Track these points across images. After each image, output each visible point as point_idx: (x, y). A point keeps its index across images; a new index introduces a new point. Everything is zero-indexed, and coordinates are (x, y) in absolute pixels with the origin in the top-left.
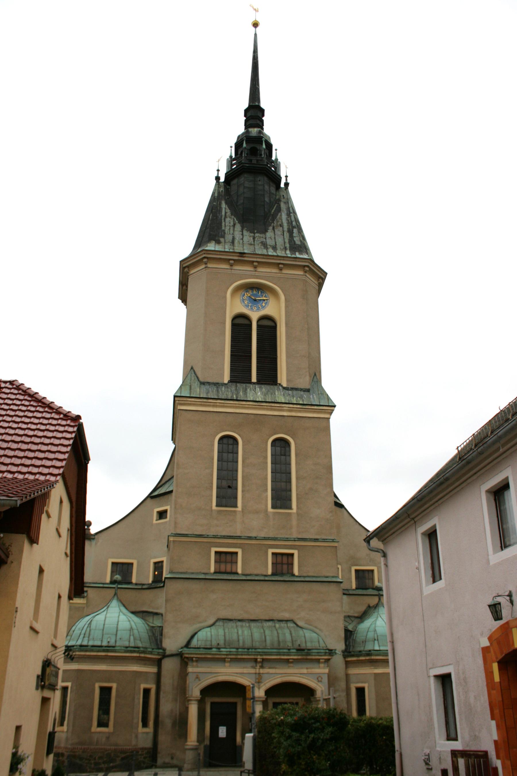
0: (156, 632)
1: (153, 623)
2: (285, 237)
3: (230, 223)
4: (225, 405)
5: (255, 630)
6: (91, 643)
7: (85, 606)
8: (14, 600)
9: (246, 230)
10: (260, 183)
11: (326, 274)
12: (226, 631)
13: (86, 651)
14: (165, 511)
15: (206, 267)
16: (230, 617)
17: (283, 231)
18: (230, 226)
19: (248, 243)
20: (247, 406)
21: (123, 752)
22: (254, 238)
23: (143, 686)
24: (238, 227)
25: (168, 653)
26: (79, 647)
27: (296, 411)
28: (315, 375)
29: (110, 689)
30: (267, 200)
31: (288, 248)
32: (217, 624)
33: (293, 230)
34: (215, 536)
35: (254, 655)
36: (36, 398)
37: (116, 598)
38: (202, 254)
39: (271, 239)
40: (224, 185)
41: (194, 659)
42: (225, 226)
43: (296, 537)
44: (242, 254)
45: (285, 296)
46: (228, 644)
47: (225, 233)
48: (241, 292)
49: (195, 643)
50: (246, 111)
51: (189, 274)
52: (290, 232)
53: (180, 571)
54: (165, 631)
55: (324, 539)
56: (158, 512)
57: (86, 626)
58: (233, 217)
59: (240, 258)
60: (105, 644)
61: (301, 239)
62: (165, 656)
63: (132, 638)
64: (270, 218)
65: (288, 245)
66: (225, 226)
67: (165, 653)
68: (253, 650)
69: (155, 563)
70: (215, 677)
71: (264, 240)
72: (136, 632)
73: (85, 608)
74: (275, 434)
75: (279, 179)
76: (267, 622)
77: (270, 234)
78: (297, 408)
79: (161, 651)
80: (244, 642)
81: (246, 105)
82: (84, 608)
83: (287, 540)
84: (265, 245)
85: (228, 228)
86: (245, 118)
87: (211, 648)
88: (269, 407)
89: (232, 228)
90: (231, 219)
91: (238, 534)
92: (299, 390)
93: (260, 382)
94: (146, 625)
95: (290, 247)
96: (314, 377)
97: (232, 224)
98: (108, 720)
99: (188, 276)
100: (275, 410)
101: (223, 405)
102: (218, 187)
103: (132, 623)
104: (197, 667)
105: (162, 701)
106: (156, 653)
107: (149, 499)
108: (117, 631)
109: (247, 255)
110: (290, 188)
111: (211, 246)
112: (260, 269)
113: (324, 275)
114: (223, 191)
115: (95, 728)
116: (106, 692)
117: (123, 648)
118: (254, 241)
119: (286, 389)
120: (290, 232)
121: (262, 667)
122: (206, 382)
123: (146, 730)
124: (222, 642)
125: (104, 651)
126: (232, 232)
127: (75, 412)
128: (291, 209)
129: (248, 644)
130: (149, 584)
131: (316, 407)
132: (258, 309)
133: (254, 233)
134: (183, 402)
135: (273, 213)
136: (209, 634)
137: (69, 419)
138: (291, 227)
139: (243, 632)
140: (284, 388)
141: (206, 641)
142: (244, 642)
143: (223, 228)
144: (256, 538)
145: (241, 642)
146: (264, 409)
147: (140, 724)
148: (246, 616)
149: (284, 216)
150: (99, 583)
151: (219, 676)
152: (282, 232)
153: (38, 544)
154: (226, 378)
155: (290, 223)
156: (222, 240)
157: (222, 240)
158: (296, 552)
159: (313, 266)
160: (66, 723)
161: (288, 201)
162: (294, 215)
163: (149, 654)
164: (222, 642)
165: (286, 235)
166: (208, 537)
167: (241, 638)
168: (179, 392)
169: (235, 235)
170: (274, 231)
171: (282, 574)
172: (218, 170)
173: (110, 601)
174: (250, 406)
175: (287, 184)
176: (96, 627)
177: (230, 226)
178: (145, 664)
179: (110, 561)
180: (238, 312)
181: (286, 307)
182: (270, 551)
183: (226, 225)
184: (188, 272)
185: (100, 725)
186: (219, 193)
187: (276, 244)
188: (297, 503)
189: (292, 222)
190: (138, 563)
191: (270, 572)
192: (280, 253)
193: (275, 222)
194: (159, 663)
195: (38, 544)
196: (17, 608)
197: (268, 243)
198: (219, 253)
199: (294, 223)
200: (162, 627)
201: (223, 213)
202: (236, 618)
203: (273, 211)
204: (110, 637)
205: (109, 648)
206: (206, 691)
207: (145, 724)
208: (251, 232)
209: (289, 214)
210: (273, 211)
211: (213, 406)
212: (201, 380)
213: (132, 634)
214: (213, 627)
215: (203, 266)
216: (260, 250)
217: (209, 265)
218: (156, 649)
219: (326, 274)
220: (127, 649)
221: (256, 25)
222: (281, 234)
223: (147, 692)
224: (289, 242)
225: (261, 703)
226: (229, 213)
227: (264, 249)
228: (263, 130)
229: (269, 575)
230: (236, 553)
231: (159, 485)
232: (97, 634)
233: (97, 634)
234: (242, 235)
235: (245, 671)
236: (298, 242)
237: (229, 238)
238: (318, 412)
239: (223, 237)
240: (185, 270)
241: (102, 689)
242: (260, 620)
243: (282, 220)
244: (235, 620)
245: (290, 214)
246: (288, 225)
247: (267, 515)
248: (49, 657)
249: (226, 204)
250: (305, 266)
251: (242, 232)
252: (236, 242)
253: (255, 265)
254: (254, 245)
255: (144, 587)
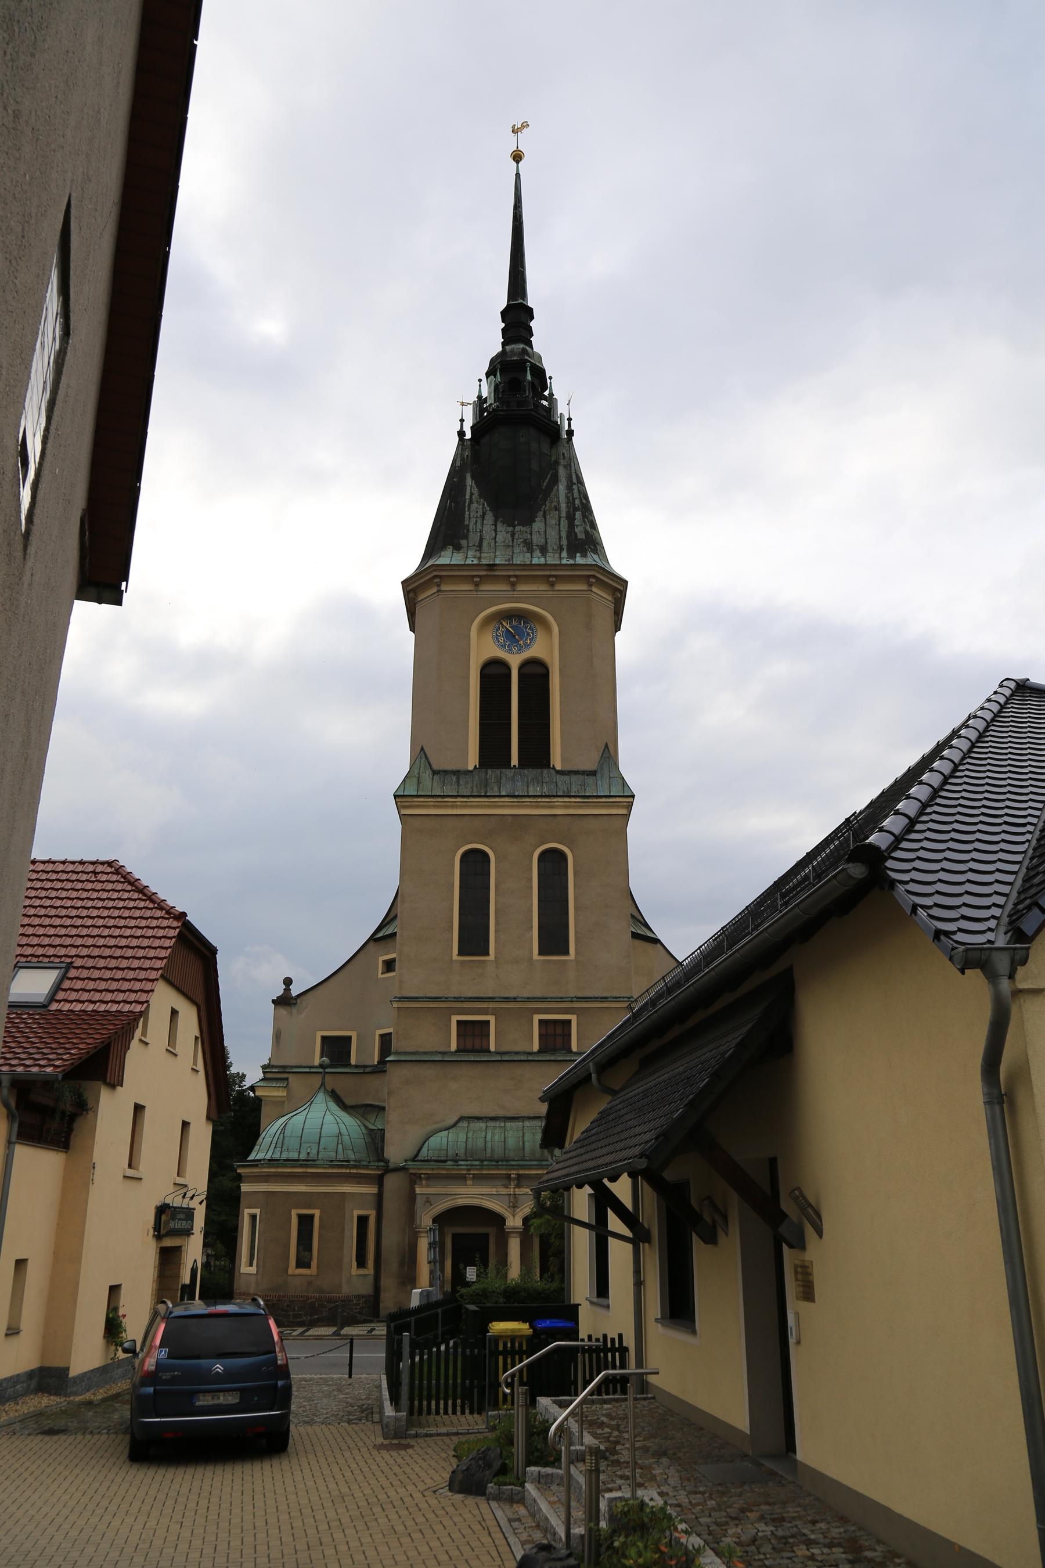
0: (375, 1137)
1: (374, 1124)
2: (562, 529)
3: (477, 512)
4: (469, 804)
5: (510, 1134)
6: (284, 1156)
7: (285, 1099)
8: (91, 1155)
9: (501, 522)
10: (522, 440)
11: (627, 582)
12: (470, 1135)
13: (278, 1167)
14: (393, 960)
15: (438, 591)
16: (477, 1114)
17: (560, 518)
18: (477, 517)
19: (503, 544)
20: (500, 804)
21: (330, 1300)
22: (513, 535)
23: (356, 1213)
24: (489, 518)
25: (391, 1165)
26: (267, 1162)
27: (573, 807)
28: (606, 746)
29: (311, 1217)
30: (535, 466)
31: (565, 547)
32: (460, 1124)
33: (575, 515)
34: (457, 998)
35: (506, 1169)
36: (136, 888)
37: (322, 1089)
38: (431, 572)
39: (539, 533)
40: (471, 445)
41: (422, 1176)
42: (470, 518)
43: (574, 996)
44: (491, 567)
45: (558, 625)
46: (470, 1154)
47: (468, 531)
48: (494, 625)
49: (424, 1153)
50: (504, 314)
51: (416, 602)
52: (571, 518)
53: (408, 1050)
54: (387, 1135)
55: (616, 998)
56: (384, 961)
57: (279, 1131)
58: (482, 500)
59: (489, 573)
60: (303, 1156)
61: (588, 528)
62: (388, 1170)
63: (340, 1146)
64: (540, 497)
65: (564, 542)
66: (470, 518)
67: (388, 1166)
68: (504, 1163)
69: (382, 1036)
70: (453, 1199)
71: (529, 536)
72: (346, 1138)
73: (286, 1102)
74: (543, 843)
75: (557, 428)
76: (531, 1120)
77: (538, 525)
78: (575, 802)
79: (382, 1164)
80: (492, 1150)
81: (503, 304)
82: (284, 1102)
83: (561, 1000)
84: (529, 546)
85: (473, 520)
86: (503, 325)
87: (445, 1161)
88: (533, 804)
89: (479, 521)
90: (480, 504)
91: (490, 995)
92: (580, 774)
93: (523, 763)
94: (362, 1128)
95: (567, 545)
96: (604, 750)
97: (480, 513)
98: (311, 1259)
99: (415, 604)
100: (543, 807)
101: (465, 804)
102: (462, 450)
103: (342, 1126)
104: (428, 1186)
105: (385, 1233)
106: (375, 1167)
107: (371, 944)
108: (320, 1137)
109: (498, 568)
110: (575, 439)
111: (446, 558)
112: (521, 587)
113: (622, 585)
114: (470, 455)
115: (292, 1269)
116: (306, 1221)
117: (326, 1162)
118: (513, 541)
119: (560, 774)
120: (571, 518)
121: (518, 1186)
122: (441, 771)
123: (362, 1271)
124: (462, 1152)
125: (301, 1166)
126: (479, 527)
127: (180, 909)
128: (574, 476)
129: (499, 1153)
130: (373, 1066)
131: (604, 800)
132: (520, 649)
133: (514, 526)
134: (407, 804)
135: (546, 487)
136: (445, 1140)
137: (171, 918)
138: (572, 510)
139: (493, 1134)
140: (558, 772)
141: (440, 1150)
142: (492, 1150)
143: (466, 523)
144: (515, 999)
145: (489, 1150)
146: (526, 807)
147: (355, 1264)
148: (501, 1113)
149: (562, 487)
150: (305, 1067)
151: (458, 1198)
152: (558, 519)
153: (122, 1086)
154: (472, 761)
155: (571, 502)
156: (464, 542)
157: (464, 542)
158: (573, 1018)
159: (605, 576)
160: (255, 1262)
161: (571, 462)
162: (578, 487)
163: (363, 1169)
164: (462, 1152)
165: (564, 523)
166: (446, 999)
167: (489, 1145)
168: (402, 788)
169: (484, 532)
170: (545, 519)
171: (554, 1050)
172: (462, 420)
173: (314, 1095)
174: (506, 804)
175: (570, 433)
176: (292, 1132)
177: (477, 517)
178: (359, 1183)
179: (319, 1034)
180: (486, 658)
181: (561, 644)
182: (537, 1018)
183: (472, 516)
184: (414, 599)
185: (299, 1265)
186: (462, 459)
187: (546, 542)
188: (576, 945)
189: (574, 499)
190: (358, 1036)
191: (536, 1047)
192: (552, 559)
193: (547, 503)
194: (380, 1181)
195: (122, 1086)
196: (94, 1163)
197: (535, 542)
198: (456, 568)
199: (577, 502)
200: (384, 1130)
201: (468, 496)
202: (487, 1116)
203: (545, 484)
204: (310, 1147)
205: (308, 1163)
206: (443, 1220)
207: (361, 1263)
208: (509, 526)
209: (570, 488)
210: (545, 484)
211: (452, 807)
212: (435, 767)
213: (340, 1142)
214: (454, 1130)
215: (435, 590)
216: (521, 558)
217: (444, 588)
218: (374, 1161)
219: (625, 583)
220: (332, 1163)
221: (517, 157)
222: (556, 524)
223: (363, 1220)
224: (567, 536)
225: (518, 1235)
226: (477, 494)
227: (528, 552)
228: (531, 347)
229: (535, 1053)
230: (488, 1022)
231: (386, 922)
232: (292, 1142)
233: (292, 1142)
234: (495, 530)
235: (494, 1191)
236: (581, 536)
237: (474, 538)
238: (608, 807)
239: (466, 537)
240: (410, 596)
241: (301, 1218)
242: (521, 1117)
243: (558, 498)
244: (485, 1118)
245: (572, 486)
246: (568, 507)
247: (532, 964)
248: (167, 1202)
249: (472, 480)
250: (589, 576)
251: (496, 526)
252: (485, 544)
253: (513, 582)
254: (513, 546)
255: (367, 1070)
